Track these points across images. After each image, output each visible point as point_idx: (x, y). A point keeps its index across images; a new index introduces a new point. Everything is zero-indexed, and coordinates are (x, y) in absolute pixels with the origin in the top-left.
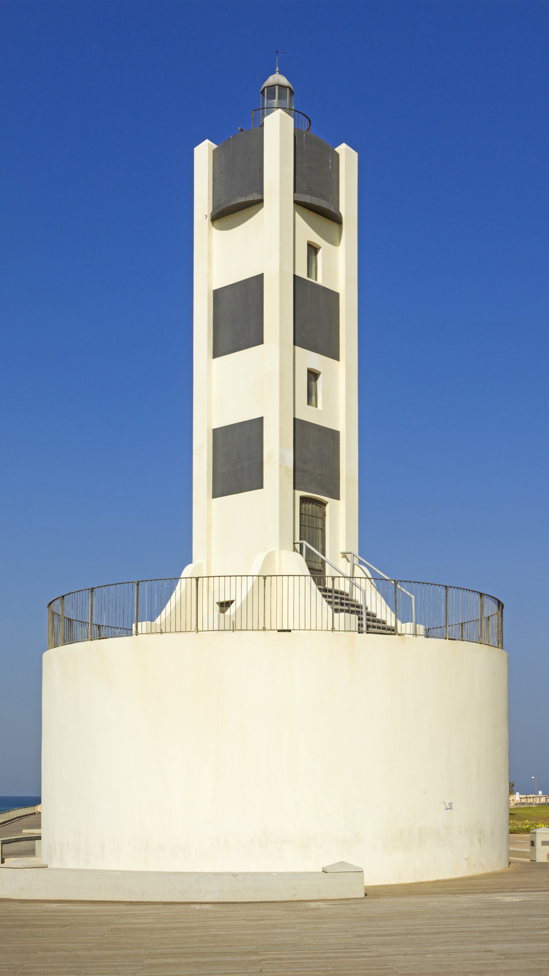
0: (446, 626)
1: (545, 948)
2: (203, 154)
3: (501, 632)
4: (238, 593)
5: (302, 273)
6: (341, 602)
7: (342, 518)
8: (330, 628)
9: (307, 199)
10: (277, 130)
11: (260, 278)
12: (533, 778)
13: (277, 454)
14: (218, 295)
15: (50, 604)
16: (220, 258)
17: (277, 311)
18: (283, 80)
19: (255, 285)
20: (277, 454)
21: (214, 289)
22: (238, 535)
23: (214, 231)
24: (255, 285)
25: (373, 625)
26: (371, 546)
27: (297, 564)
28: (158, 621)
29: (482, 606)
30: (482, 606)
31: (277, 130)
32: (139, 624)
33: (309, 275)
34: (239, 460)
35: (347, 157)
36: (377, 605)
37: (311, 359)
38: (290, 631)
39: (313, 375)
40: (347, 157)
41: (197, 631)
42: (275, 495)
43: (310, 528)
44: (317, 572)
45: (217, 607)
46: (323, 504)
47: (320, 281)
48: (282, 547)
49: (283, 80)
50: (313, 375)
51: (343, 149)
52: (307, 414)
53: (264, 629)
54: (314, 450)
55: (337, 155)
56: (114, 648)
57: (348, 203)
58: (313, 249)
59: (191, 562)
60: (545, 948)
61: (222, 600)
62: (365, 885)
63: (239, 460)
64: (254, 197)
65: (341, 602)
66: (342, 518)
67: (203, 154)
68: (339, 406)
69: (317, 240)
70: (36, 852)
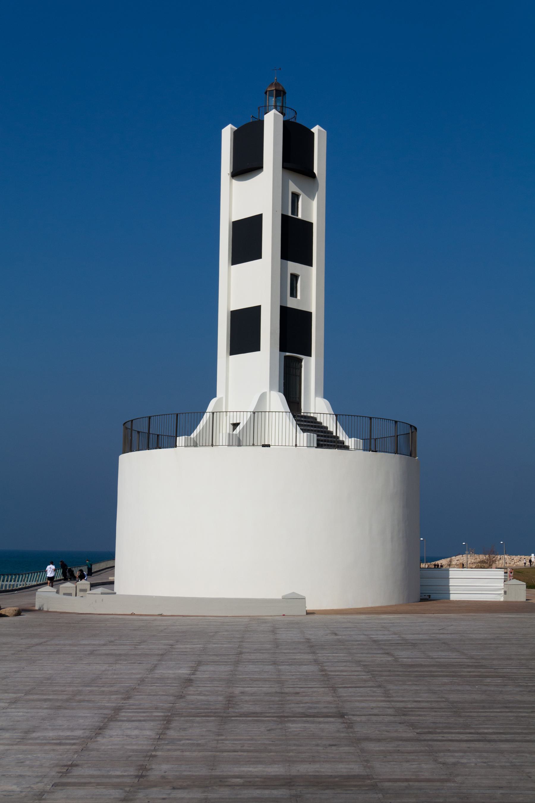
0: (397, 436)
1: (62, 642)
4: (243, 420)
6: (307, 424)
8: (294, 445)
12: (422, 539)
15: (124, 424)
17: (270, 238)
22: (245, 381)
23: (234, 182)
25: (326, 440)
27: (277, 401)
28: (192, 436)
32: (178, 438)
34: (245, 332)
37: (293, 267)
38: (269, 446)
41: (212, 445)
45: (232, 427)
46: (300, 360)
47: (300, 216)
48: (271, 389)
50: (294, 278)
51: (316, 130)
52: (292, 303)
53: (253, 445)
55: (313, 134)
57: (319, 165)
58: (295, 197)
59: (216, 396)
60: (62, 642)
61: (235, 422)
62: (307, 609)
63: (245, 332)
65: (307, 424)
68: (311, 296)
69: (297, 190)
70: (419, 559)
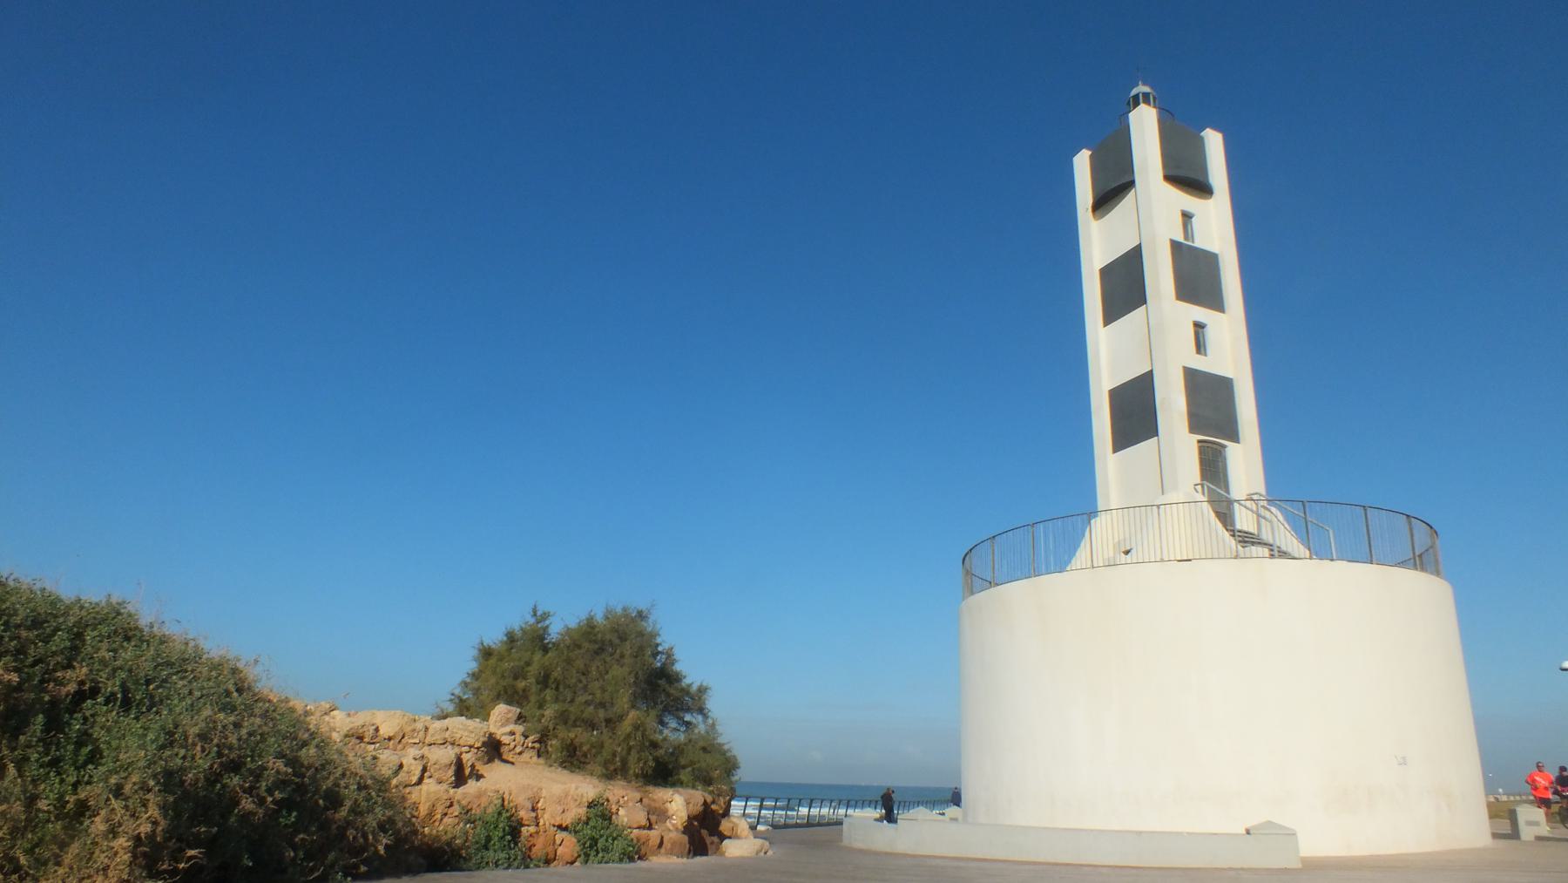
2: (1082, 162)
3: (1437, 561)
5: (1180, 238)
7: (1245, 464)
9: (1182, 173)
10: (1144, 124)
11: (1106, 323)
13: (1172, 403)
14: (1224, 447)
16: (1099, 242)
18: (1146, 89)
19: (1110, 315)
20: (1172, 403)
21: (1141, 310)
24: (1110, 315)
26: (1282, 488)
29: (1411, 530)
30: (1411, 530)
31: (1144, 124)
33: (1186, 238)
34: (1135, 413)
35: (1214, 142)
36: (1286, 538)
39: (1199, 327)
40: (1214, 142)
42: (1177, 437)
43: (1213, 467)
44: (1226, 518)
49: (1146, 89)
54: (1210, 403)
56: (1049, 583)
63: (1135, 413)
64: (1126, 179)
66: (1245, 464)
67: (1082, 162)
